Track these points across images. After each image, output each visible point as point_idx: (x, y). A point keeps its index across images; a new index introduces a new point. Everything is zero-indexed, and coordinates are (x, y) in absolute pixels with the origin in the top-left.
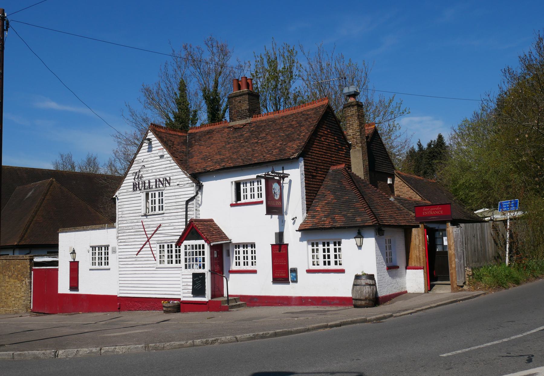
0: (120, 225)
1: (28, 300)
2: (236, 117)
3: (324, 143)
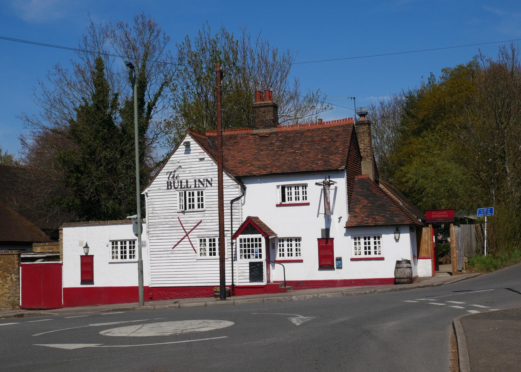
0: (150, 221)
2: (260, 126)
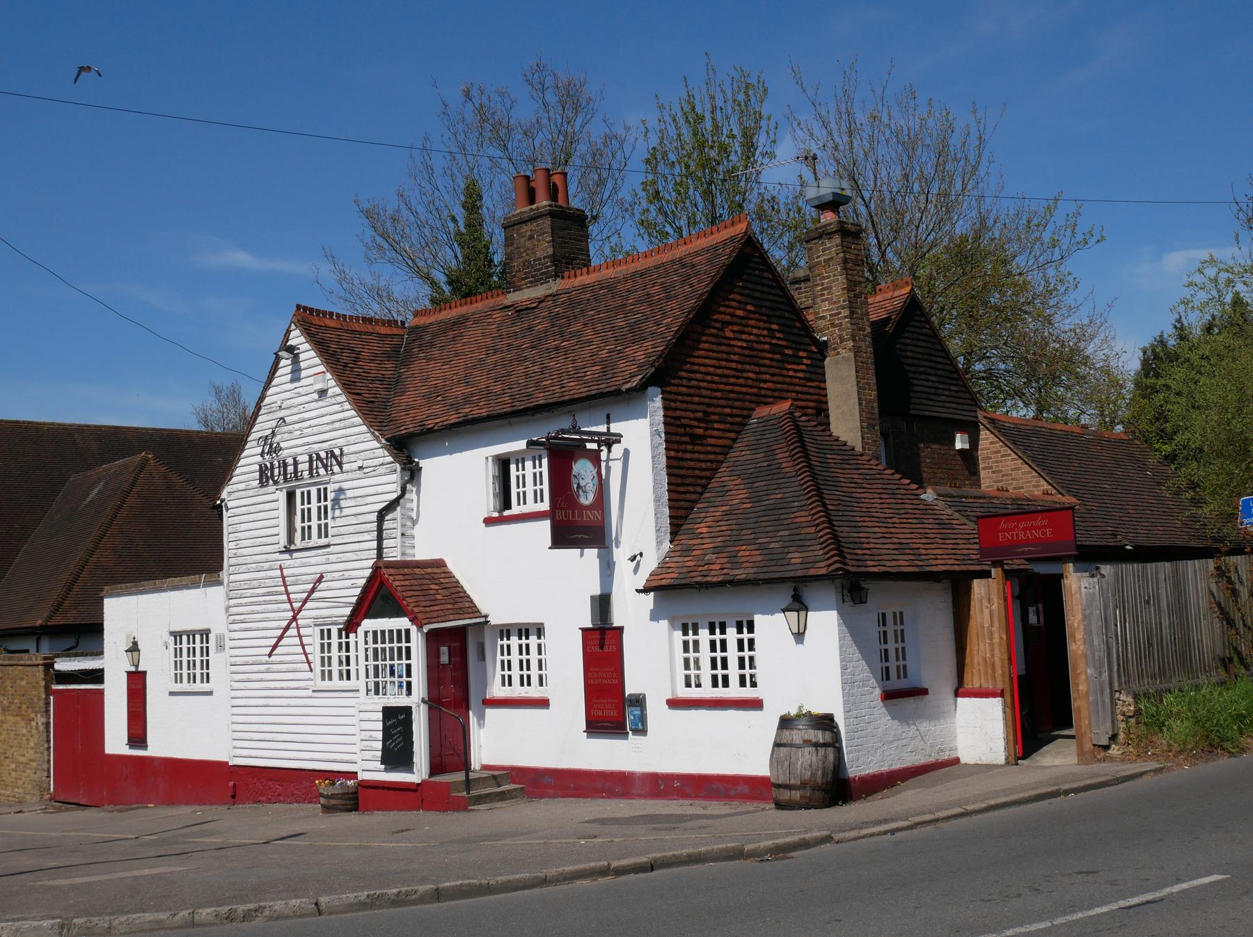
0: (232, 578)
1: (43, 770)
3: (732, 343)
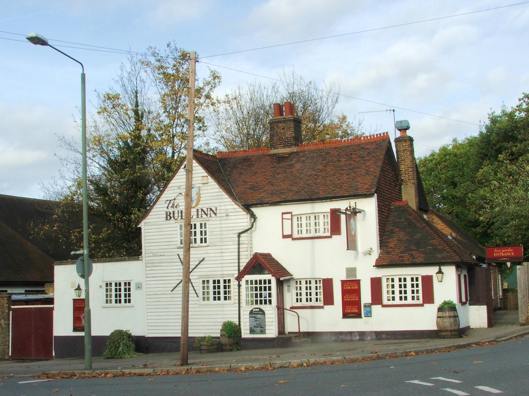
0: (147, 259)
